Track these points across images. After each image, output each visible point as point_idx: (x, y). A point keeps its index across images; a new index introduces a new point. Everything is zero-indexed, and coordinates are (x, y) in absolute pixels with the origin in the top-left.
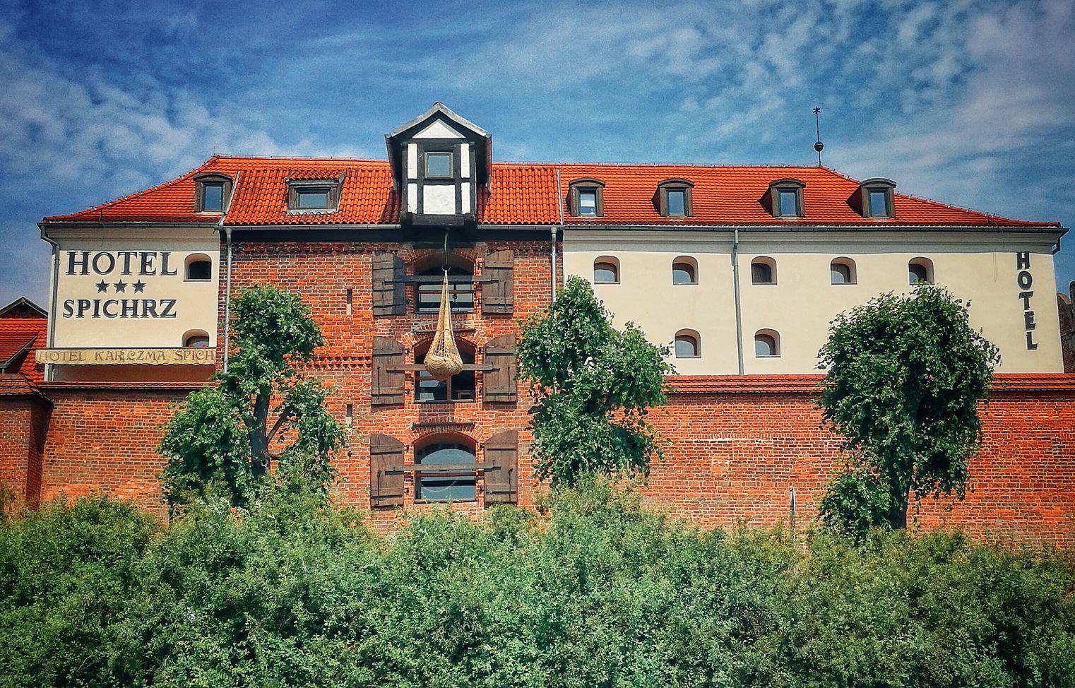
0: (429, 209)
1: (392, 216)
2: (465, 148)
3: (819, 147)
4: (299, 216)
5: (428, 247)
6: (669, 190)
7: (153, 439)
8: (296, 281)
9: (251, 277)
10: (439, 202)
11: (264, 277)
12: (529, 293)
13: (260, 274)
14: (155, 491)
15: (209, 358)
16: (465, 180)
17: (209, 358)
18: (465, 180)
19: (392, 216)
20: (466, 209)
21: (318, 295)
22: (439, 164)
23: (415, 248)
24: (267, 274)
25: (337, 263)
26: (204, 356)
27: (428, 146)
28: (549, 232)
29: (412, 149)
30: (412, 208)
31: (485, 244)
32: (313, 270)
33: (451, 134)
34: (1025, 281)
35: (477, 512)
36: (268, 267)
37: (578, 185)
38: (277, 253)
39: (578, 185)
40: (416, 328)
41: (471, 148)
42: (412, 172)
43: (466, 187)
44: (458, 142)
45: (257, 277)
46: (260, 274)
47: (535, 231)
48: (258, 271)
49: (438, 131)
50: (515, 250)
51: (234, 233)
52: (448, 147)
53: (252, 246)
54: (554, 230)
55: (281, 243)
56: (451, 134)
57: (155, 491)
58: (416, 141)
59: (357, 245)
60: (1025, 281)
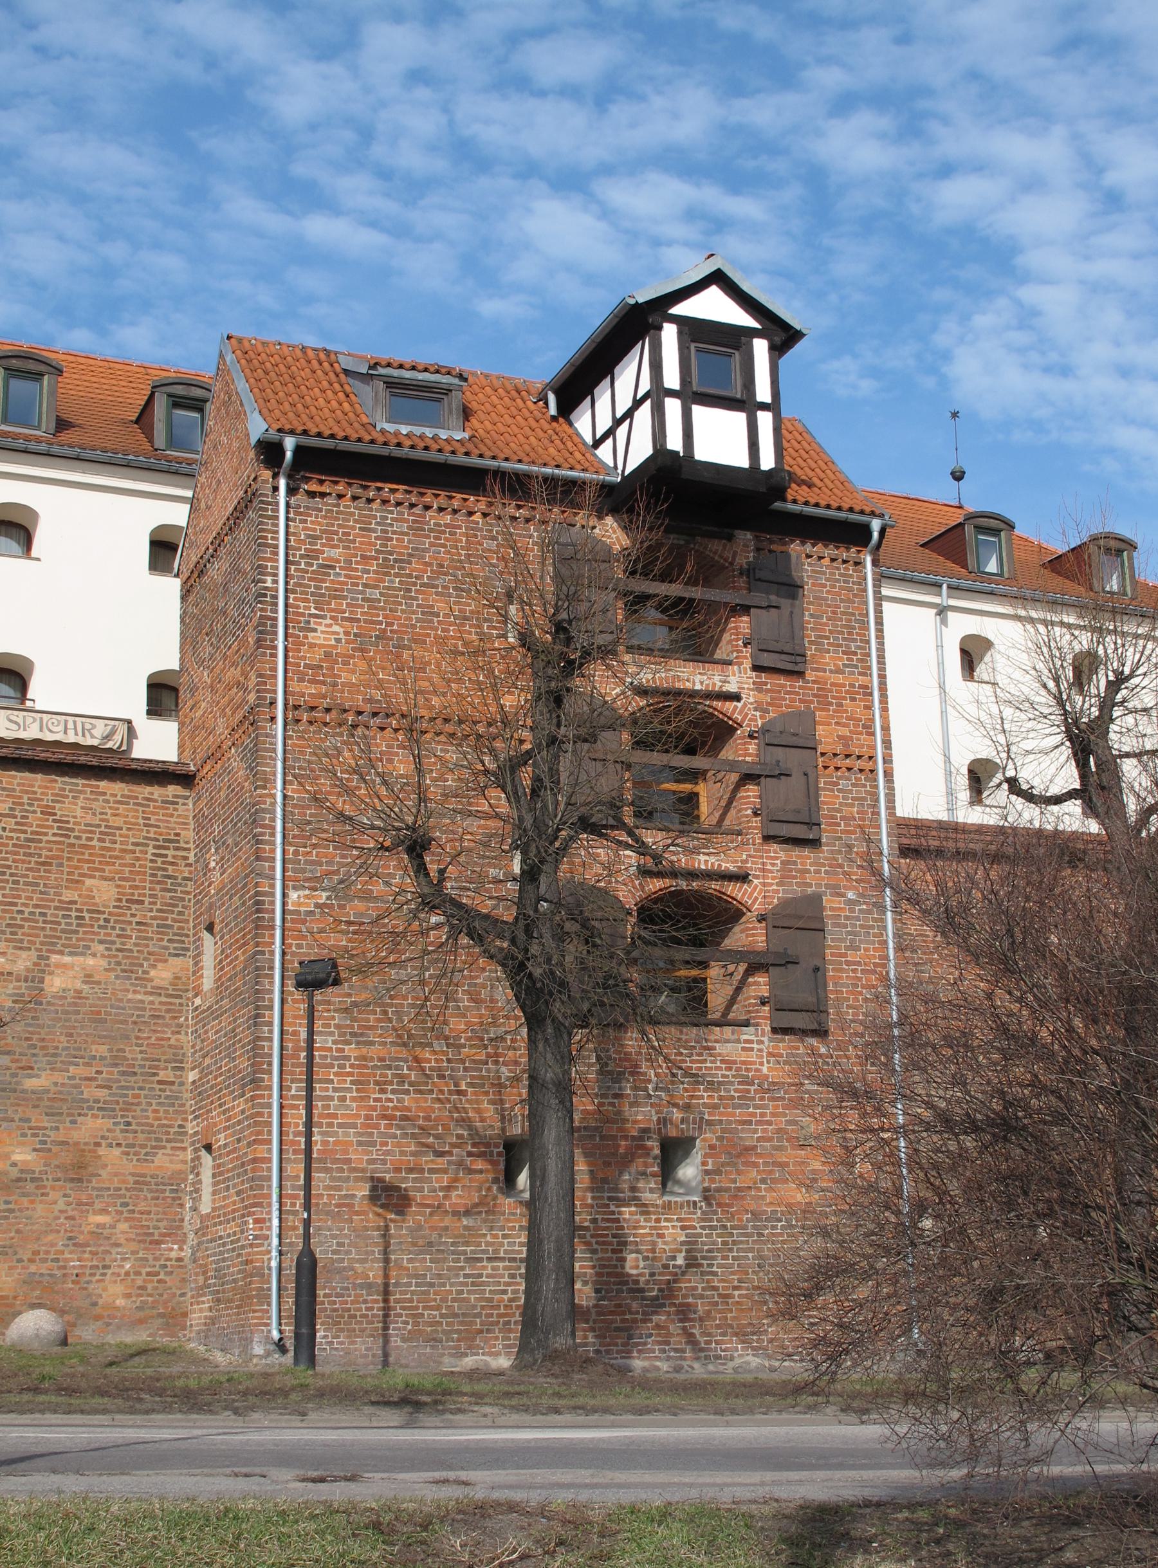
0: (701, 453)
3: (958, 476)
6: (980, 529)
7: (23, 862)
8: (410, 563)
9: (323, 545)
11: (348, 548)
12: (828, 638)
13: (340, 540)
14: (28, 970)
15: (71, 732)
17: (71, 732)
20: (767, 462)
24: (354, 542)
25: (484, 537)
26: (61, 728)
27: (696, 332)
28: (866, 530)
31: (749, 536)
33: (742, 318)
36: (353, 528)
37: (170, 389)
39: (170, 389)
43: (765, 420)
44: (752, 333)
45: (334, 546)
48: (336, 533)
49: (713, 306)
51: (299, 450)
53: (321, 482)
54: (876, 525)
56: (742, 318)
57: (28, 970)
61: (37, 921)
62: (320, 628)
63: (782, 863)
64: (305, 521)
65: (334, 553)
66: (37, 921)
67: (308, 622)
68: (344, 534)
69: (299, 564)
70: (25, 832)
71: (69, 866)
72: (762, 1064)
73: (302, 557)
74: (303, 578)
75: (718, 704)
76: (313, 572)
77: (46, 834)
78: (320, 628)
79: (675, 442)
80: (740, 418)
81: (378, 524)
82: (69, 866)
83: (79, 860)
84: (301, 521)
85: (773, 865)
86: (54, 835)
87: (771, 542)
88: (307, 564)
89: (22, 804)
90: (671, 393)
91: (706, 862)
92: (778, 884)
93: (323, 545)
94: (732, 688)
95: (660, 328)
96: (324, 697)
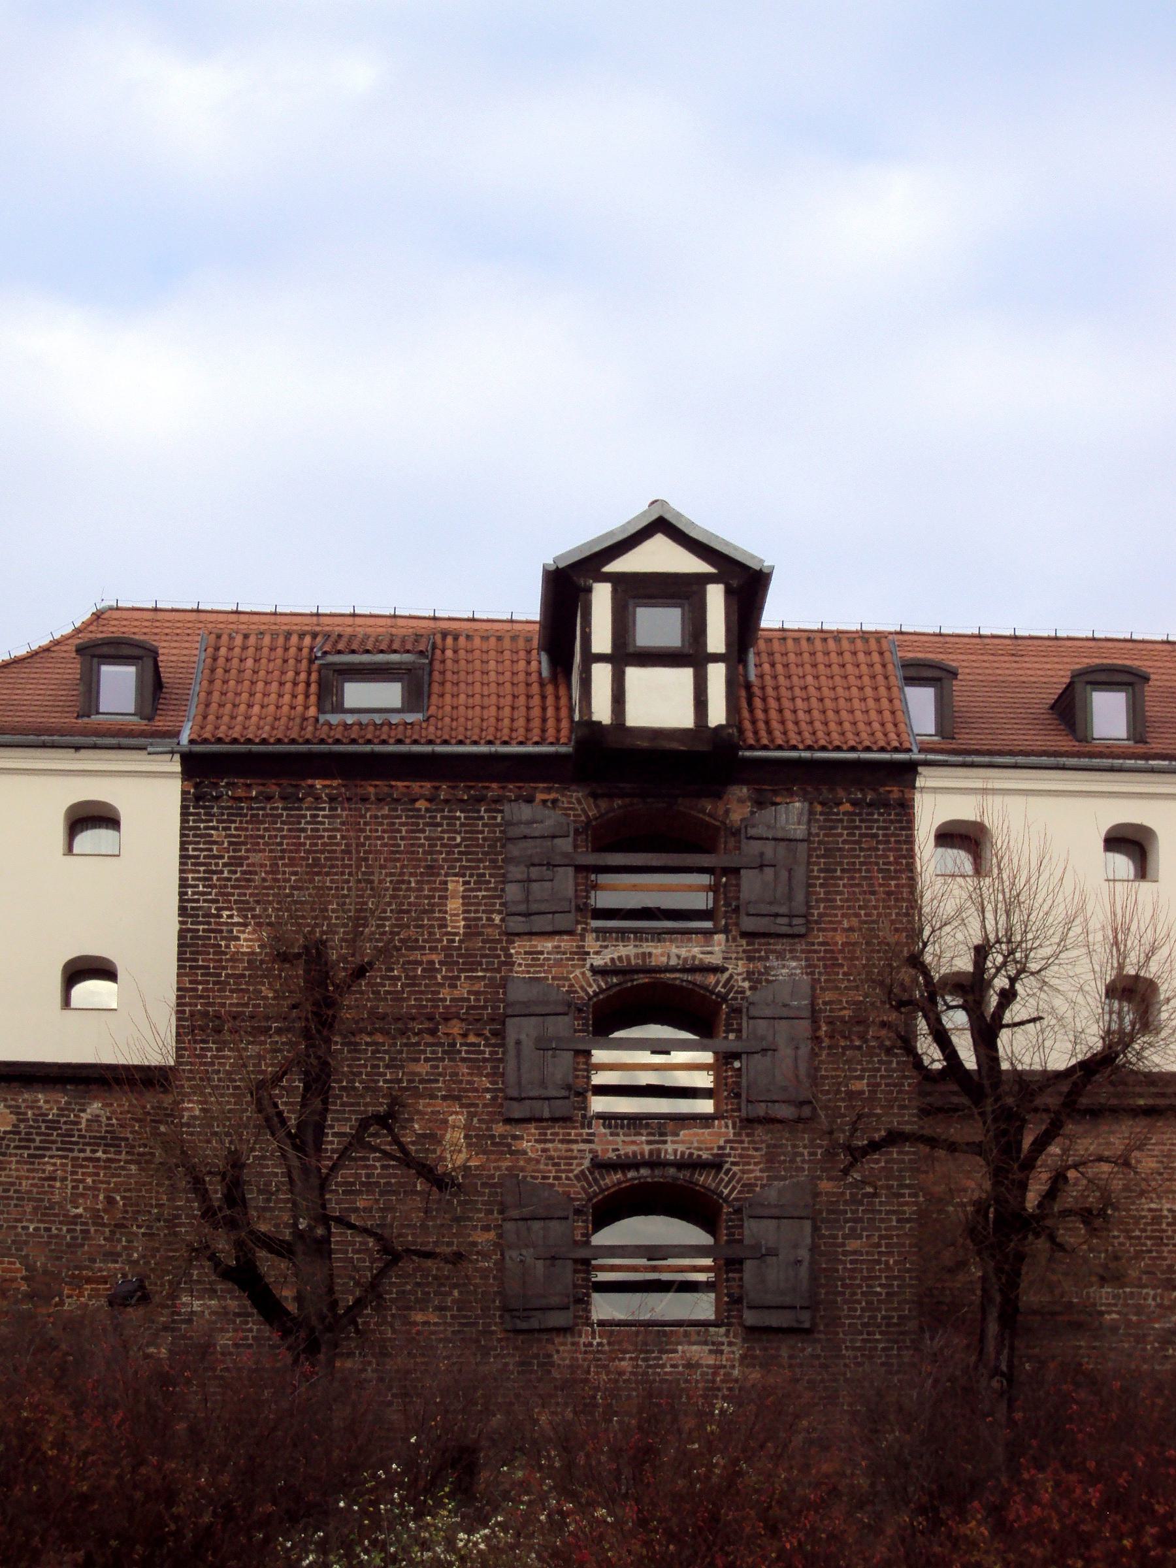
0: (638, 716)
1: (544, 731)
2: (715, 596)
4: (346, 726)
5: (621, 796)
9: (247, 851)
10: (660, 701)
13: (266, 844)
16: (716, 658)
18: (716, 658)
19: (544, 731)
20: (717, 715)
21: (11, 1198)
22: (659, 625)
23: (595, 796)
27: (637, 591)
29: (602, 597)
30: (602, 711)
32: (379, 838)
33: (692, 564)
34: (935, 790)
35: (725, 1348)
38: (301, 800)
40: (598, 961)
41: (729, 593)
42: (602, 640)
43: (717, 674)
44: (701, 580)
46: (266, 844)
47: (309, 756)
48: (263, 837)
49: (660, 557)
50: (811, 803)
52: (679, 591)
55: (310, 782)
56: (692, 564)
58: (608, 577)
59: (471, 787)
60: (935, 790)
61: (42, 1237)
62: (242, 936)
63: (768, 1147)
64: (229, 828)
65: (255, 858)
66: (42, 1237)
67: (232, 931)
68: (270, 837)
69: (222, 872)
70: (28, 1148)
71: (73, 1181)
72: (733, 1367)
73: (225, 865)
74: (226, 886)
75: (698, 978)
76: (237, 880)
77: (49, 1149)
78: (242, 936)
79: (602, 711)
80: (685, 675)
81: (307, 823)
82: (73, 1181)
83: (83, 1174)
84: (225, 829)
85: (756, 1149)
86: (58, 1149)
87: (775, 792)
88: (230, 872)
89: (27, 1120)
90: (601, 658)
91: (675, 1151)
92: (761, 1171)
93: (247, 851)
94: (716, 959)
95: (589, 590)
96: (246, 1005)
